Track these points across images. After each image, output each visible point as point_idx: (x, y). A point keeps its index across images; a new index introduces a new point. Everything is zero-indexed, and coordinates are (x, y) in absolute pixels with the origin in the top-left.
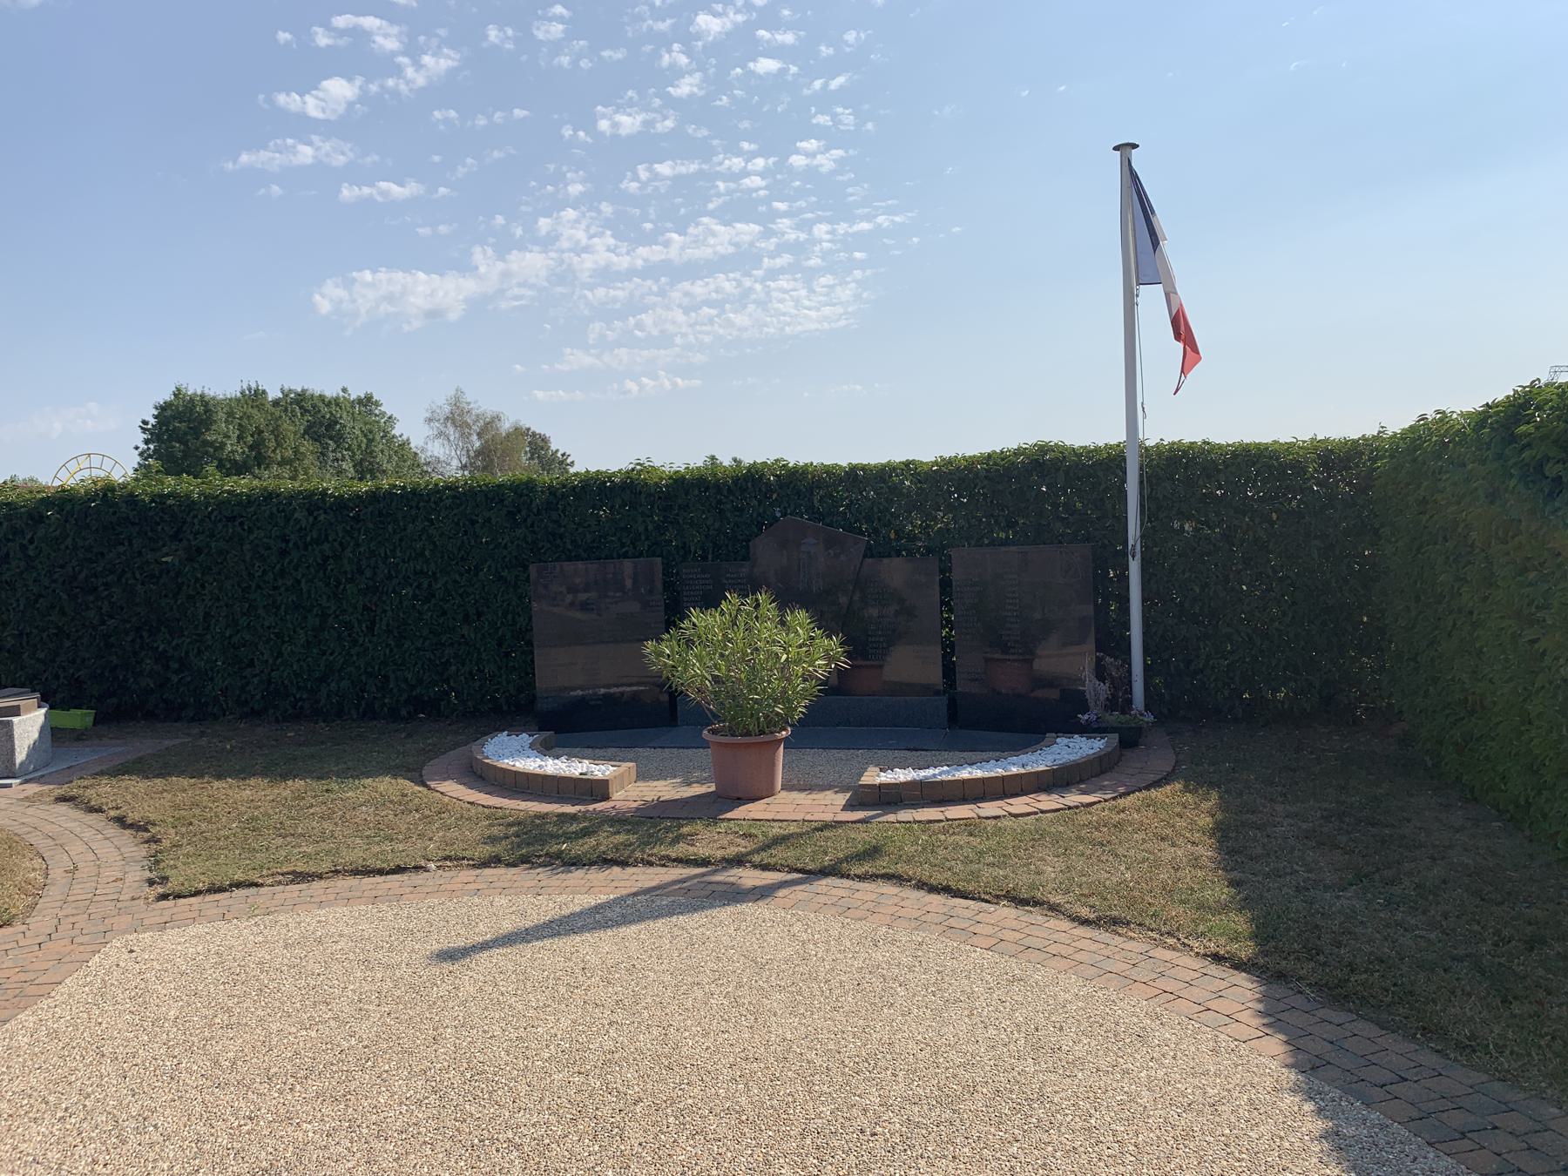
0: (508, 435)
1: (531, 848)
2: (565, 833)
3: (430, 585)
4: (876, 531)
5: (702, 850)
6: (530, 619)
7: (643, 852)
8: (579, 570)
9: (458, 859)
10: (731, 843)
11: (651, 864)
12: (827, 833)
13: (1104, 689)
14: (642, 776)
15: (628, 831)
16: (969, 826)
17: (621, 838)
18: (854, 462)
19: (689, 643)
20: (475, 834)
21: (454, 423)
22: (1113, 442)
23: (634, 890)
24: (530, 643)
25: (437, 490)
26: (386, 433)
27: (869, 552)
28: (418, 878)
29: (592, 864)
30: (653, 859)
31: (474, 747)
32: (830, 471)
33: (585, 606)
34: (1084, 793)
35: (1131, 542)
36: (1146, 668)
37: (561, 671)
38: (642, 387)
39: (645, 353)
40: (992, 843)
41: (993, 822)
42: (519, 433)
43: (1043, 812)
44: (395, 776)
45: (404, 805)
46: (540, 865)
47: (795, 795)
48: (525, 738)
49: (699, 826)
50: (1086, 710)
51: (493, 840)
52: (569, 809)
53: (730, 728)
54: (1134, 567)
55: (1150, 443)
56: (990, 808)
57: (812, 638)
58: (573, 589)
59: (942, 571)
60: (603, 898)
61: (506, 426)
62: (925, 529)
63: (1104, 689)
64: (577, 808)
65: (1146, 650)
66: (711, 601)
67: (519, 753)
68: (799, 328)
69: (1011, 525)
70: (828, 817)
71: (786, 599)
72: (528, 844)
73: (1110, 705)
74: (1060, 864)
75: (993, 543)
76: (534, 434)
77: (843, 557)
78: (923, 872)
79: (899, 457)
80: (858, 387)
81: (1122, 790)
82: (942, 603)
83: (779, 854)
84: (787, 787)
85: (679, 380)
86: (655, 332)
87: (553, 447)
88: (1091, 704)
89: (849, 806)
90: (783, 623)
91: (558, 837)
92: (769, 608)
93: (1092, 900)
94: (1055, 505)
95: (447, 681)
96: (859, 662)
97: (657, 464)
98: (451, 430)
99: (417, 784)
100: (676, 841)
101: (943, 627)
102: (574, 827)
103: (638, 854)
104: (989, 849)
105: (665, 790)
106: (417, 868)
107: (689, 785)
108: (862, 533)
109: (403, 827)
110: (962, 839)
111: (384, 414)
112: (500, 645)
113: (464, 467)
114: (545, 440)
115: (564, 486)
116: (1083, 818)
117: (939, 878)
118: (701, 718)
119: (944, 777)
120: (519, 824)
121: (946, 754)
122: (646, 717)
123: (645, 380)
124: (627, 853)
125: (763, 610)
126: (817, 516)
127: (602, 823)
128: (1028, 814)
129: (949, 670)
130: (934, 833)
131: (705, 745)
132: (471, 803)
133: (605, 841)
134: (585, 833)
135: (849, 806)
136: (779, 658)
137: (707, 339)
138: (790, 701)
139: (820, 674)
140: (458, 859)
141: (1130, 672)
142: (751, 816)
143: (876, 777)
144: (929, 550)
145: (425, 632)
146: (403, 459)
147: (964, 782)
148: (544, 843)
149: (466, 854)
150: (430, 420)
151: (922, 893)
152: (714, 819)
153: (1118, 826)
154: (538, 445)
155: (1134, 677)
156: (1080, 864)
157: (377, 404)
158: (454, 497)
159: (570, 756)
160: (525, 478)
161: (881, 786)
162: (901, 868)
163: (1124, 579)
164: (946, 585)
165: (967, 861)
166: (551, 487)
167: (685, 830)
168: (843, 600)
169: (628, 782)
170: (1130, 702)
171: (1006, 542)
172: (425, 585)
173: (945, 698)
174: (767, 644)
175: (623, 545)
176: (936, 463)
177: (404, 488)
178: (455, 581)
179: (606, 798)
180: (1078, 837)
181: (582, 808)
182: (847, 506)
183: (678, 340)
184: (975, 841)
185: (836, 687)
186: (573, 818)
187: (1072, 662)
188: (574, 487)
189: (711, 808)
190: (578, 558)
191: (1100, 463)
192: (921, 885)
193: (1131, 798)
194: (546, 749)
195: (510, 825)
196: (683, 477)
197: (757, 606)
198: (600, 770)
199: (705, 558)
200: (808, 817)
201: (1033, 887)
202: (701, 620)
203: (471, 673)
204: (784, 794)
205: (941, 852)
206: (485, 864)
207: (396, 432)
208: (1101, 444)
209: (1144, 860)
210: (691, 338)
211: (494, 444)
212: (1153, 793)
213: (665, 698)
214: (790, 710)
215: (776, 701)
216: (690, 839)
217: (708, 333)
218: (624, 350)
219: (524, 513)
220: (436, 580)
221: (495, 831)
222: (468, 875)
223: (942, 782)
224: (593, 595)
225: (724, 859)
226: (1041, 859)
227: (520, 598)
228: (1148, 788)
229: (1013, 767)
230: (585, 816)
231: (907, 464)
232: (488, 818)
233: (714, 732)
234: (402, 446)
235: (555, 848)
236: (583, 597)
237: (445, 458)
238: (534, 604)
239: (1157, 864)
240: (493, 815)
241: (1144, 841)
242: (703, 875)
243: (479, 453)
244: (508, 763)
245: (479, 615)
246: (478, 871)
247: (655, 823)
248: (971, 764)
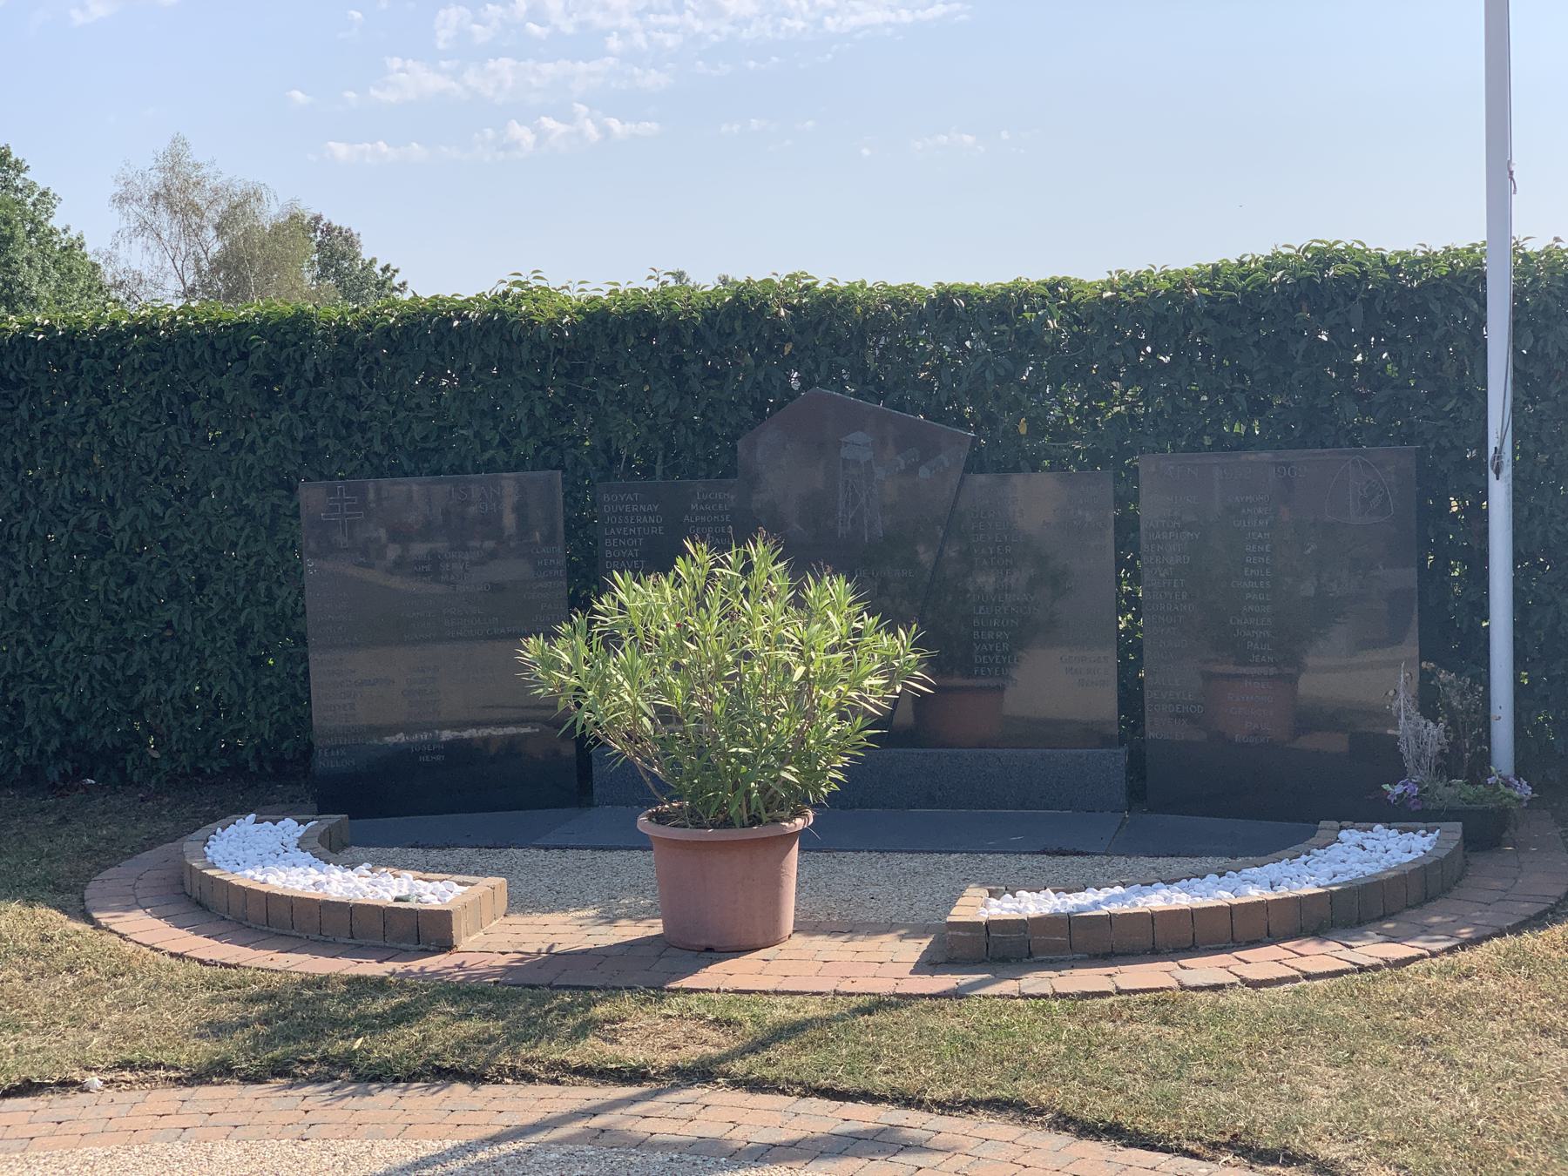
0: (277, 229)
1: (294, 1046)
2: (361, 1017)
3: (103, 524)
4: (990, 419)
5: (631, 1052)
6: (301, 593)
7: (514, 1053)
8: (413, 496)
9: (145, 1066)
10: (689, 1037)
11: (529, 1078)
12: (877, 1018)
13: (1434, 733)
14: (519, 903)
15: (487, 1014)
16: (1162, 1004)
17: (472, 1027)
18: (949, 281)
19: (611, 641)
20: (181, 1018)
21: (170, 205)
22: (1463, 244)
23: (494, 1130)
24: (301, 639)
25: (115, 335)
26: (37, 225)
27: (975, 463)
28: (71, 1103)
29: (411, 1077)
30: (533, 1069)
31: (189, 845)
32: (899, 300)
33: (432, 567)
34: (1392, 938)
35: (1493, 443)
36: (1519, 692)
37: (362, 693)
38: (541, 136)
39: (548, 68)
40: (1207, 1038)
41: (1210, 997)
42: (298, 226)
43: (1308, 977)
44: (30, 902)
45: (44, 958)
46: (310, 1080)
47: (820, 942)
48: (290, 828)
49: (627, 1003)
50: (1398, 775)
51: (217, 1029)
52: (372, 968)
53: (692, 812)
54: (1499, 494)
55: (1532, 247)
56: (1204, 969)
57: (858, 633)
58: (399, 535)
59: (1120, 501)
60: (431, 1147)
61: (271, 212)
62: (1088, 415)
63: (1434, 733)
64: (389, 966)
65: (1520, 659)
66: (656, 559)
67: (278, 855)
68: (853, 20)
69: (1257, 408)
70: (884, 987)
71: (804, 560)
72: (287, 1039)
73: (1448, 765)
74: (1341, 1084)
75: (1225, 445)
76: (329, 230)
77: (924, 472)
78: (1068, 1097)
79: (1035, 272)
80: (968, 139)
81: (1466, 933)
82: (1120, 563)
83: (784, 1060)
84: (806, 927)
85: (615, 124)
86: (568, 28)
87: (366, 255)
88: (1410, 765)
89: (928, 965)
90: (799, 603)
91: (347, 1024)
92: (769, 569)
93: (1401, 1154)
94: (1347, 369)
95: (138, 713)
96: (957, 681)
97: (554, 283)
98: (164, 217)
99: (72, 916)
100: (581, 1032)
101: (1122, 612)
102: (380, 1005)
103: (505, 1059)
104: (1201, 1051)
105: (569, 931)
106: (65, 1085)
107: (612, 921)
108: (962, 423)
109: (41, 1003)
110: (1148, 1031)
111: (31, 187)
112: (242, 643)
113: (190, 292)
114: (349, 240)
115: (369, 327)
116: (1388, 989)
117: (1099, 1108)
118: (635, 789)
119: (1115, 908)
120: (271, 997)
121: (1121, 862)
122: (528, 786)
123: (548, 123)
124: (481, 1057)
125: (759, 575)
126: (873, 389)
127: (433, 999)
128: (1280, 981)
129: (1131, 698)
130: (1094, 1019)
131: (643, 844)
132: (179, 956)
133: (441, 1032)
134: (401, 1016)
135: (928, 965)
136: (788, 669)
137: (671, 41)
138: (811, 758)
139: (874, 704)
140: (145, 1066)
141: (1486, 700)
142: (731, 984)
143: (978, 906)
144: (1096, 458)
145: (94, 616)
146: (69, 275)
147: (1153, 917)
148: (318, 1035)
149: (163, 1056)
150: (122, 200)
151: (1064, 1139)
152: (658, 991)
153: (1457, 1005)
154: (335, 252)
155: (1495, 711)
156: (1380, 1082)
157: (18, 167)
158: (149, 348)
159: (377, 863)
160: (289, 311)
161: (990, 926)
162: (1025, 1089)
163: (1478, 517)
164: (1127, 528)
165: (1157, 1074)
166: (342, 329)
167: (600, 1011)
168: (925, 556)
169: (489, 915)
170: (1486, 758)
171: (1245, 443)
172: (93, 524)
173: (1119, 756)
174: (769, 642)
175: (485, 445)
176: (1110, 285)
177: (49, 329)
178: (154, 516)
179: (446, 946)
180: (1378, 1027)
181: (398, 966)
182: (935, 371)
183: (614, 43)
184: (1173, 1035)
185: (900, 732)
186: (380, 985)
187: (1376, 680)
188: (388, 330)
189: (649, 969)
190: (395, 471)
191: (1434, 285)
192: (1065, 1122)
193: (1484, 949)
194: (332, 849)
195: (253, 1000)
196: (605, 311)
197: (748, 569)
198: (431, 891)
199: (648, 472)
200: (845, 987)
201: (1285, 1126)
202: (636, 597)
203: (186, 698)
204: (798, 940)
205: (1105, 1055)
206: (198, 1077)
207: (55, 222)
208: (1438, 248)
209: (1508, 1074)
210: (639, 39)
211: (244, 255)
212: (1528, 939)
213: (569, 750)
214: (812, 777)
215: (783, 759)
216: (609, 1029)
217: (673, 30)
218: (506, 63)
219: (288, 380)
220: (115, 514)
221: (224, 1012)
222: (168, 1097)
223: (1111, 916)
224: (441, 545)
225: (675, 1070)
226: (1304, 1071)
227: (281, 549)
228: (1517, 930)
229: (1253, 886)
230: (402, 983)
231: (1053, 286)
232: (209, 985)
233: (660, 819)
234: (68, 249)
235: (340, 1047)
236: (419, 549)
237: (146, 271)
238: (310, 564)
239: (1531, 1083)
240: (221, 980)
241: (1507, 1035)
242: (633, 1101)
243: (219, 264)
244: (254, 877)
245: (201, 583)
246: (187, 1091)
247: (544, 994)
248: (1169, 882)
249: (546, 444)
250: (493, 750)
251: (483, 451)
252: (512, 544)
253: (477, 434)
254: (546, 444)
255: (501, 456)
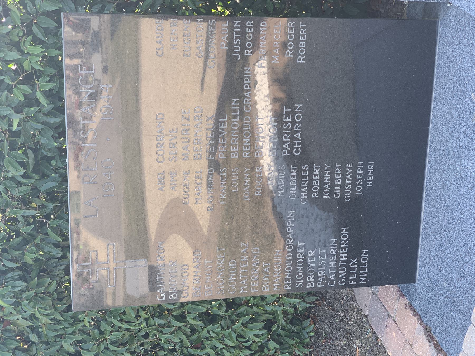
33: (95, 96)
175: (31, 101)
249: (30, 32)
250: (281, 95)
251: (38, 103)
252: (85, 61)
253: (18, 110)
254: (30, 32)
255: (43, 85)
